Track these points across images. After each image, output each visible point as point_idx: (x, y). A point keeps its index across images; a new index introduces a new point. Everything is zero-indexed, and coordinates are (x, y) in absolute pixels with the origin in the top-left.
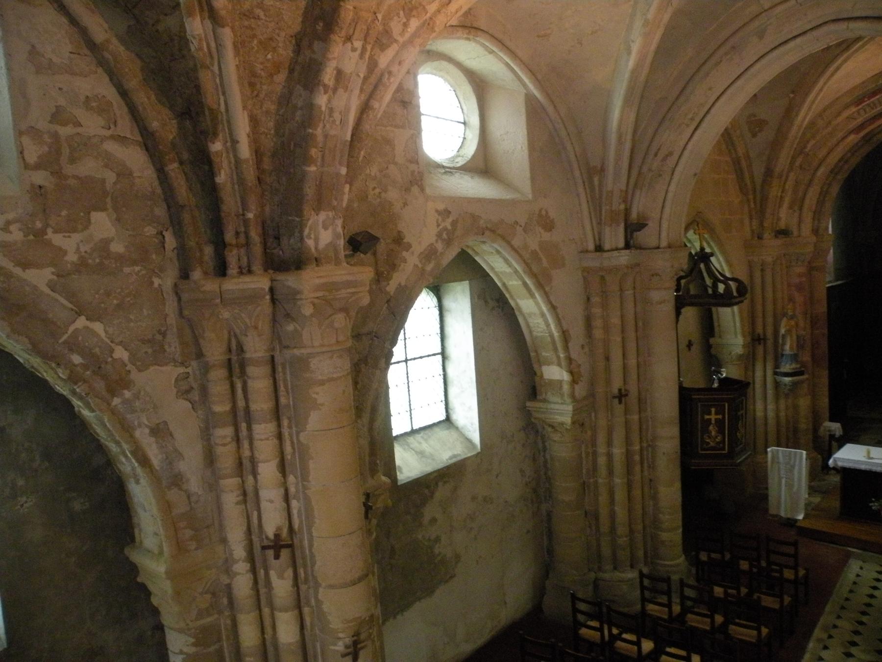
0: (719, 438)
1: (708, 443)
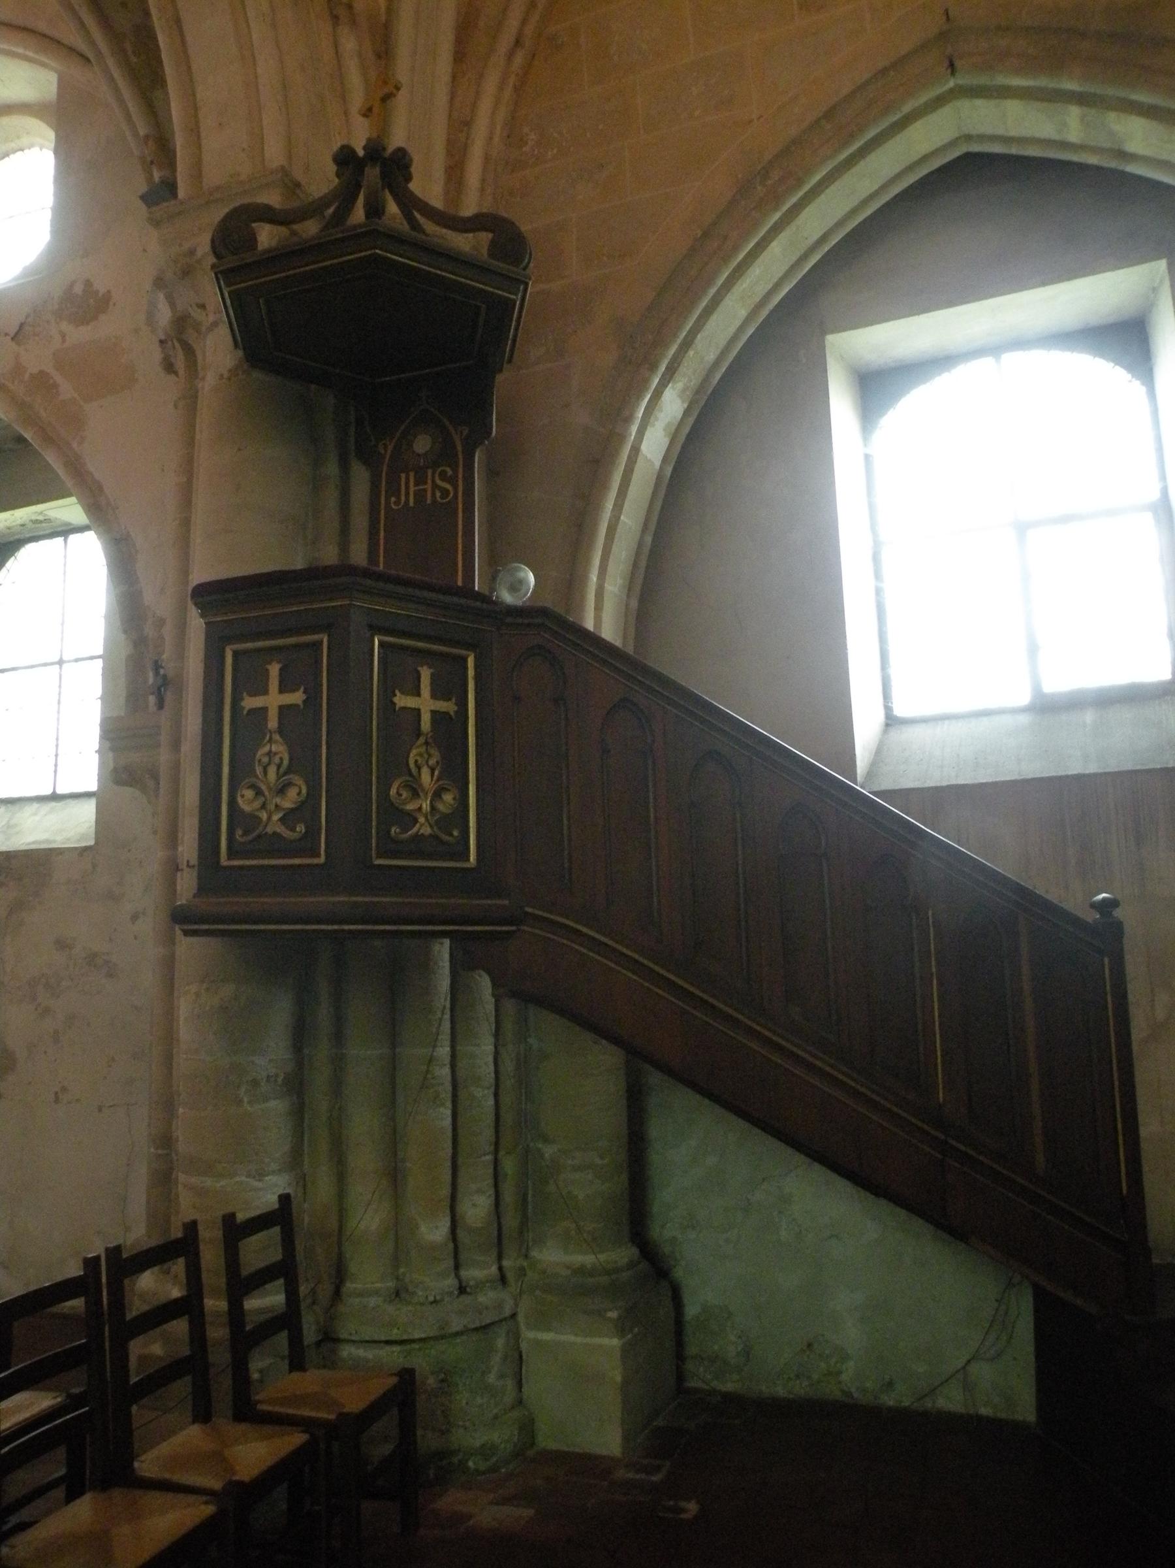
0: (292, 793)
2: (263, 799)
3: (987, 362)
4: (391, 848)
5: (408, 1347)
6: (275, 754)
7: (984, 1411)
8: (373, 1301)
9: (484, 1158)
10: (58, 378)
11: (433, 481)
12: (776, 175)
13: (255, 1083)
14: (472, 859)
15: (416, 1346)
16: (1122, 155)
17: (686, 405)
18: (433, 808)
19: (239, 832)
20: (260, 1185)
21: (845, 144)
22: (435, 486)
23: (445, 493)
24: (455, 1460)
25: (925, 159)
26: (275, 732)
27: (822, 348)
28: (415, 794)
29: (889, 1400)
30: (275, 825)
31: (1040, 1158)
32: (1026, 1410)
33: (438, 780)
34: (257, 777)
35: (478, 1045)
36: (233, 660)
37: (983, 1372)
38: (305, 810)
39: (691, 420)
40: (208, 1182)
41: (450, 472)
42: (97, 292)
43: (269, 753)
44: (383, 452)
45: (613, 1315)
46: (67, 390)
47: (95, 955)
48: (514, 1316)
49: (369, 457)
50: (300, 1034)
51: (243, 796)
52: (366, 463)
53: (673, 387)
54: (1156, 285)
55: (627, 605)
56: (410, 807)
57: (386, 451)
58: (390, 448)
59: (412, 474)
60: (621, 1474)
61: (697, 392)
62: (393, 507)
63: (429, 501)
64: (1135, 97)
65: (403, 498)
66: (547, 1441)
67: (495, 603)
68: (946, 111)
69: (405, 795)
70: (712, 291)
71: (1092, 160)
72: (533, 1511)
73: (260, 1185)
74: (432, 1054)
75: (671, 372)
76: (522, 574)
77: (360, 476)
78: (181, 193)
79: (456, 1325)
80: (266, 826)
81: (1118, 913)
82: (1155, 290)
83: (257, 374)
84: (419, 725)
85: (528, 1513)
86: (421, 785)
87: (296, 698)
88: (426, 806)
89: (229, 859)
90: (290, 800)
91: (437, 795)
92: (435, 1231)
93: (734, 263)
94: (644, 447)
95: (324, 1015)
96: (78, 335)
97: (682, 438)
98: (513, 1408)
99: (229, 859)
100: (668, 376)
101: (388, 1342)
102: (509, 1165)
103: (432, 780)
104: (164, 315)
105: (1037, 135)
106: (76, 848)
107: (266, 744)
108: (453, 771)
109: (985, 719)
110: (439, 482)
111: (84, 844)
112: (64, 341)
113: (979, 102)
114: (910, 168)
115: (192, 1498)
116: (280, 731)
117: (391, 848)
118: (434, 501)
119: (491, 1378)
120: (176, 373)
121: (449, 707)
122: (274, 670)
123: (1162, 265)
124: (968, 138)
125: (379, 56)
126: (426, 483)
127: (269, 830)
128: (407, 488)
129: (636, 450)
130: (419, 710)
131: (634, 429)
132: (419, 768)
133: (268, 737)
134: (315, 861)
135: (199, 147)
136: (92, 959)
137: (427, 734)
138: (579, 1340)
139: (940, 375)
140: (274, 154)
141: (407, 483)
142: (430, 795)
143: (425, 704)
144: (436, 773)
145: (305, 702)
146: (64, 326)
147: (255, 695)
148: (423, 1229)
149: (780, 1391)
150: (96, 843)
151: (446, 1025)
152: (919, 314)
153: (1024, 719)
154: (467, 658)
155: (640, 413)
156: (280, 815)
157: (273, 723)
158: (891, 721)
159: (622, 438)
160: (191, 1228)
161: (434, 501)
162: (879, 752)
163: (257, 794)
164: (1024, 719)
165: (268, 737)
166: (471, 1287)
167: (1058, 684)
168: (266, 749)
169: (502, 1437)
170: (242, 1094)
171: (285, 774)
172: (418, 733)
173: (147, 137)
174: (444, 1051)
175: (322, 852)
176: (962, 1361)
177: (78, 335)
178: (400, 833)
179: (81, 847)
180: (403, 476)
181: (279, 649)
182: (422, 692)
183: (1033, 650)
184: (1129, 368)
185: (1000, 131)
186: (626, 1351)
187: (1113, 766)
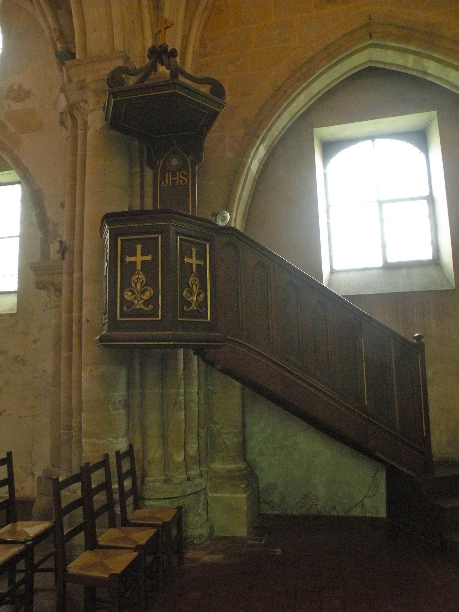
0: (148, 293)
1: (131, 303)
2: (135, 296)
3: (369, 142)
4: (184, 314)
5: (171, 500)
6: (140, 279)
7: (368, 515)
8: (158, 484)
9: (194, 430)
10: (7, 123)
11: (179, 176)
12: (305, 70)
13: (114, 403)
14: (209, 319)
15: (174, 500)
16: (425, 73)
17: (266, 152)
18: (197, 300)
19: (125, 308)
20: (116, 441)
21: (331, 60)
22: (180, 179)
23: (184, 181)
24: (190, 540)
25: (355, 67)
26: (139, 270)
27: (312, 133)
28: (191, 294)
29: (334, 513)
30: (139, 305)
31: (398, 424)
32: (383, 513)
33: (199, 289)
34: (133, 287)
35: (193, 388)
36: (121, 243)
37: (367, 502)
38: (152, 300)
39: (266, 157)
40: (97, 441)
41: (186, 173)
42: (24, 89)
43: (137, 279)
44: (158, 164)
45: (243, 486)
46: (11, 129)
47: (18, 356)
48: (205, 488)
49: (152, 164)
50: (130, 384)
51: (127, 294)
52: (152, 168)
53: (263, 146)
54: (431, 119)
55: (242, 226)
56: (189, 299)
57: (159, 164)
58: (161, 162)
59: (170, 173)
60: (249, 542)
61: (270, 147)
62: (163, 185)
63: (178, 184)
64: (435, 55)
65: (167, 182)
66: (218, 533)
67: (216, 225)
68: (366, 52)
69: (188, 294)
70: (280, 110)
71: (415, 74)
72: (223, 556)
73: (116, 441)
74: (178, 392)
75: (263, 139)
76: (225, 215)
77: (149, 174)
78: (78, 57)
79: (189, 492)
80: (136, 305)
81: (422, 340)
82: (431, 121)
83: (111, 131)
84: (192, 270)
85: (220, 556)
86: (193, 292)
87: (148, 258)
88: (195, 299)
89: (121, 318)
90: (146, 296)
91: (198, 295)
92: (179, 458)
93: (289, 101)
94: (252, 167)
95: (137, 378)
96: (16, 106)
97: (263, 164)
98: (206, 522)
99: (121, 318)
100: (263, 140)
101: (164, 499)
102: (202, 433)
103: (196, 289)
104: (63, 103)
105: (397, 63)
106: (8, 314)
107: (136, 275)
108: (203, 288)
109: (367, 271)
110: (181, 177)
111: (12, 312)
112: (10, 108)
113: (378, 50)
114: (350, 70)
115: (128, 551)
116: (142, 270)
117: (184, 314)
118: (179, 184)
119: (200, 511)
120: (66, 127)
121: (201, 263)
122: (139, 247)
123: (435, 113)
124: (372, 61)
125: (155, 8)
126: (176, 177)
127: (138, 307)
128: (169, 179)
129: (249, 168)
130: (192, 264)
131: (250, 160)
132: (192, 285)
133: (137, 272)
134: (157, 319)
135: (85, 38)
136: (16, 358)
137: (195, 272)
138: (230, 496)
139: (352, 145)
140: (118, 45)
141: (169, 177)
142: (196, 295)
143: (194, 261)
144: (198, 287)
145: (152, 259)
146: (10, 102)
147: (131, 256)
148: (175, 457)
149: (295, 513)
150: (17, 312)
151: (182, 382)
152: (348, 123)
153: (380, 272)
154: (206, 245)
155: (252, 155)
156: (142, 301)
157: (139, 267)
158: (332, 271)
159: (246, 163)
160: (106, 456)
161: (179, 184)
162: (329, 282)
163: (133, 294)
164: (380, 272)
165: (137, 272)
166: (191, 478)
167: (392, 259)
168: (137, 276)
169: (204, 531)
170: (110, 407)
171: (144, 286)
172: (192, 272)
173: (55, 29)
174: (182, 390)
175: (160, 315)
176: (361, 498)
177: (16, 106)
178: (187, 309)
179: (10, 314)
180: (167, 174)
181: (142, 239)
182: (193, 257)
183: (384, 247)
184: (420, 147)
185: (384, 60)
186: (248, 499)
187: (415, 289)
